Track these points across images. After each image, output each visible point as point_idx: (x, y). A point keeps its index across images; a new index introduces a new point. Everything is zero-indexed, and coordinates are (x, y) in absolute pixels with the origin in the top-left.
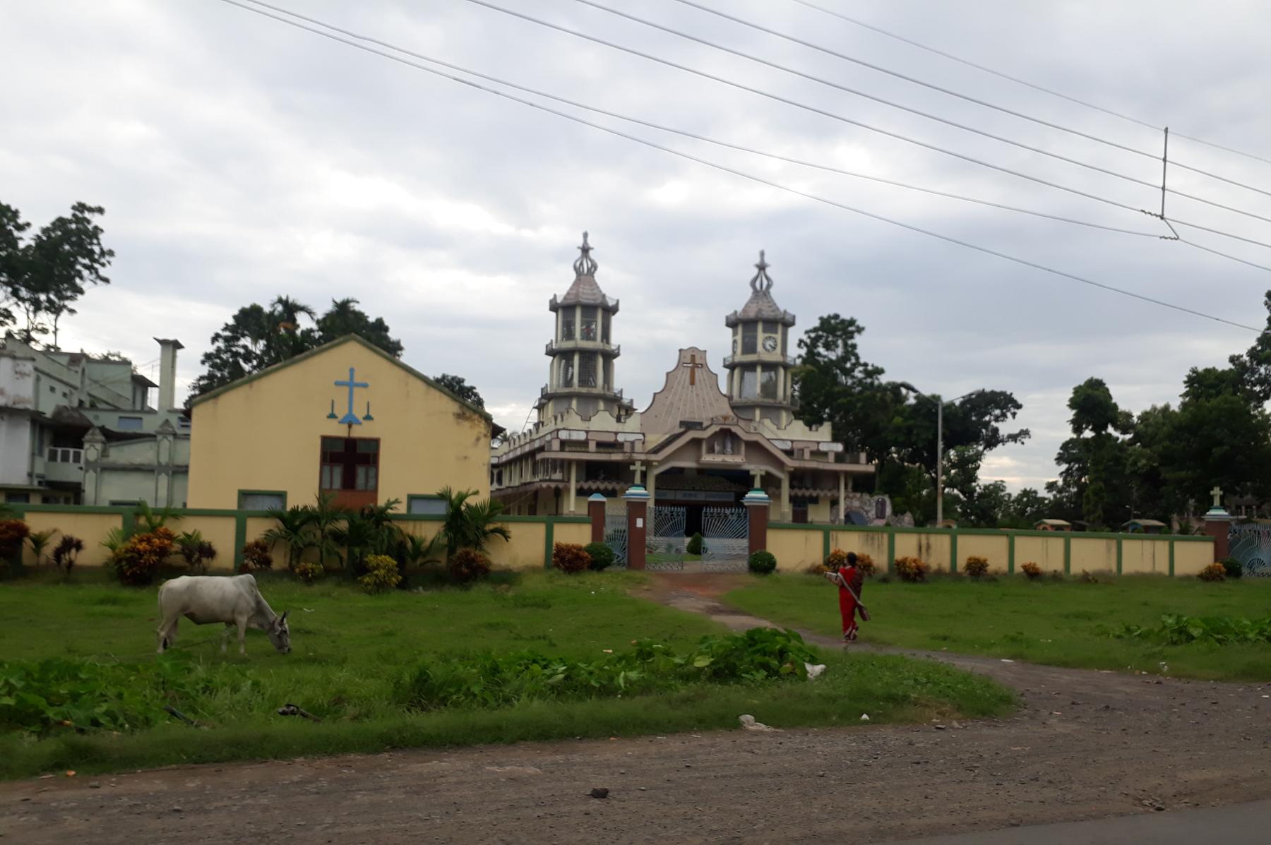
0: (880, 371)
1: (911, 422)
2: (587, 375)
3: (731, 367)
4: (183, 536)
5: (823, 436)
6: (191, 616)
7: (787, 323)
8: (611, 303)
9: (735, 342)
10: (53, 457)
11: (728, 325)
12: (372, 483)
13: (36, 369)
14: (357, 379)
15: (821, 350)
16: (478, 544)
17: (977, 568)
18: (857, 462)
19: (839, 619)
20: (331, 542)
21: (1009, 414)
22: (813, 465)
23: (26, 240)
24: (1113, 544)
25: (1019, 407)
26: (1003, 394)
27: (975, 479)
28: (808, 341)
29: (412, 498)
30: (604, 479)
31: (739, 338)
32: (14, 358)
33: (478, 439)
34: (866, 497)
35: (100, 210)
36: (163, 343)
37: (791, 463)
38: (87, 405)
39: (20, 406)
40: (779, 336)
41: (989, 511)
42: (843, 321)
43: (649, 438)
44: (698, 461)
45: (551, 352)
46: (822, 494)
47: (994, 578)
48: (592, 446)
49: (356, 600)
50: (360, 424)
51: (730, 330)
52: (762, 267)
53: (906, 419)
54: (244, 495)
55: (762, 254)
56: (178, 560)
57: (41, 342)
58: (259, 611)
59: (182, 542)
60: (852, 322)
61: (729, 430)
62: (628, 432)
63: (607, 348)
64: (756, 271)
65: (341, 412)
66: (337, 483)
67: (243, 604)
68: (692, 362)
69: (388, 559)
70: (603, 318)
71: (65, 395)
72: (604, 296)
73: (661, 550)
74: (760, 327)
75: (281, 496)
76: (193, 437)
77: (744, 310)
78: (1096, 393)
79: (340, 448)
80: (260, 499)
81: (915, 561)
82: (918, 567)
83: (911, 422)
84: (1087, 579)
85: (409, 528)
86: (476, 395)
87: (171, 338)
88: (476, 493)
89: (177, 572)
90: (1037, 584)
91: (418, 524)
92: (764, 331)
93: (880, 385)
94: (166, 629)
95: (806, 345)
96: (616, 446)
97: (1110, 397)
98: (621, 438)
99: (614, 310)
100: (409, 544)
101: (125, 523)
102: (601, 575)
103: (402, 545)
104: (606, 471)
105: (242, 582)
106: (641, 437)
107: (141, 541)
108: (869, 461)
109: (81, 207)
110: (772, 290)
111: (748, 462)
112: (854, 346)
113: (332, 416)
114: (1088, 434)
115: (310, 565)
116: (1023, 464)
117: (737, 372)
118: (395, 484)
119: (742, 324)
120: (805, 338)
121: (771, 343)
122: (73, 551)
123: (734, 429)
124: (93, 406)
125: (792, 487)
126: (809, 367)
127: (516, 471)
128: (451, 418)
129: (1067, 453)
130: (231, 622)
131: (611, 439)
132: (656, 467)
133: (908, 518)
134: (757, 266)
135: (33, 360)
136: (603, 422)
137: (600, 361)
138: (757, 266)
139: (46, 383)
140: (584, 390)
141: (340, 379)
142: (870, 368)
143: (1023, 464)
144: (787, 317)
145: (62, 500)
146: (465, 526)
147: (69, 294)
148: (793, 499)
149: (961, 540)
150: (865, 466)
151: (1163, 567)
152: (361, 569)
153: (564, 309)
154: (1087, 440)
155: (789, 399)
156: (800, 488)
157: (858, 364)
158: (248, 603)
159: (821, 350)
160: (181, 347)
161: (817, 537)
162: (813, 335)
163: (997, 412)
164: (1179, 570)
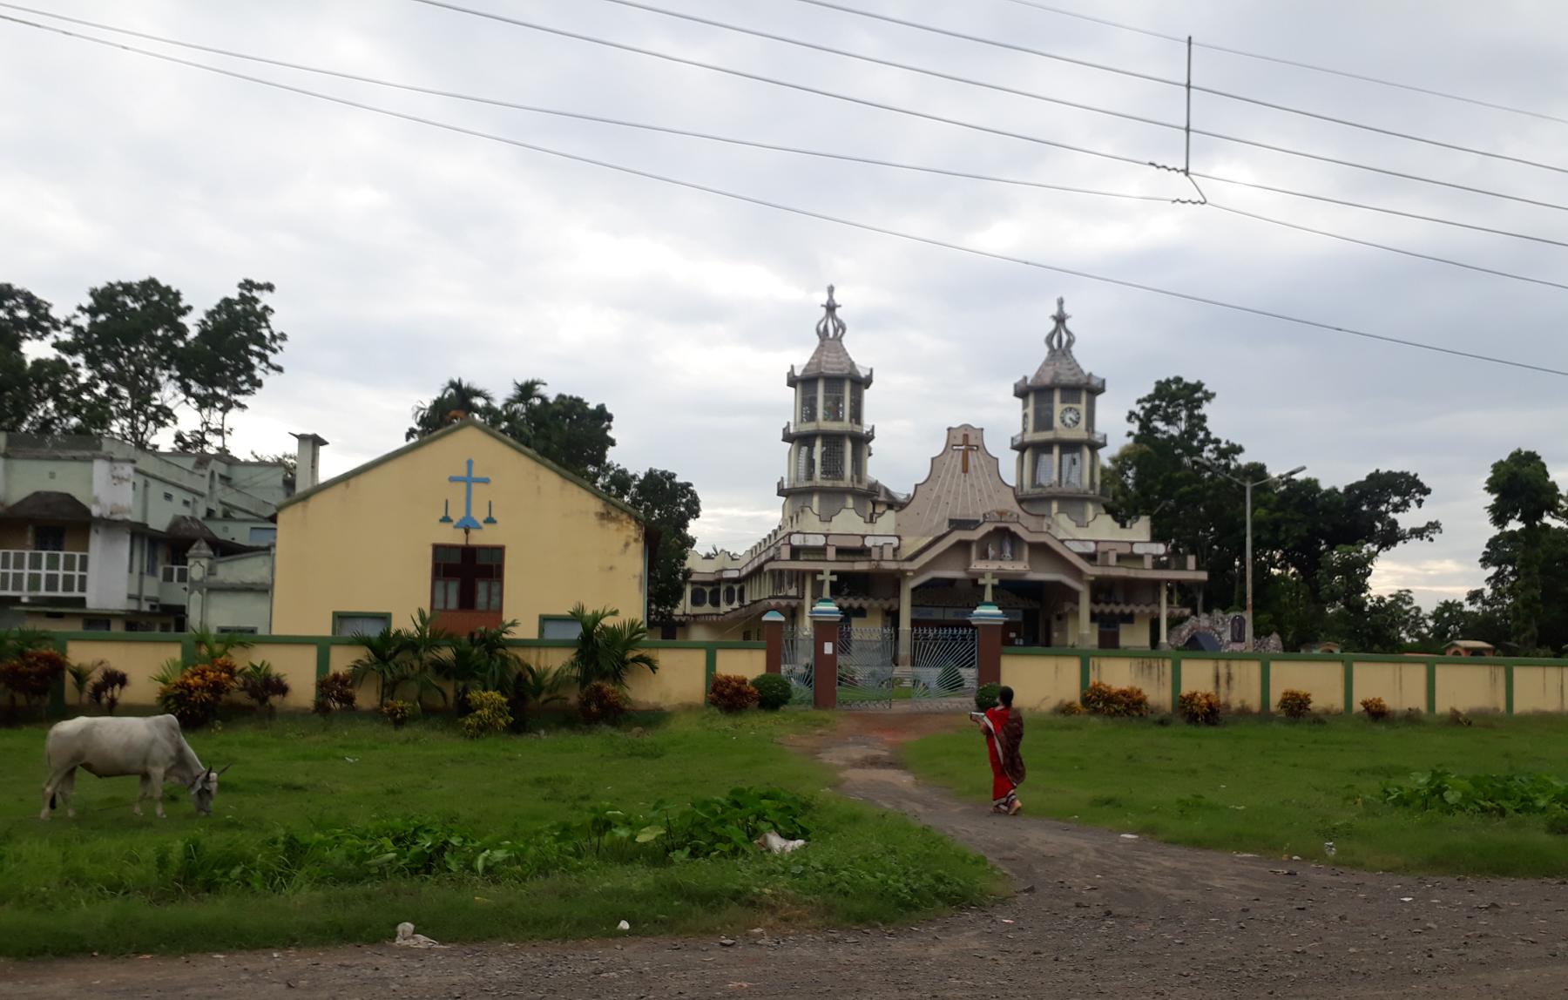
0: (1240, 450)
1: (1278, 515)
2: (832, 466)
3: (1021, 448)
4: (249, 669)
5: (1139, 532)
6: (88, 767)
7: (1093, 389)
8: (863, 374)
9: (1025, 416)
10: (168, 577)
11: (1016, 395)
12: (495, 600)
13: (137, 471)
14: (475, 474)
15: (1160, 425)
16: (617, 677)
17: (1296, 706)
18: (1183, 567)
19: (987, 776)
20: (429, 675)
21: (1412, 503)
22: (1122, 572)
23: (192, 324)
24: (1500, 672)
25: (1427, 492)
26: (1404, 475)
27: (1365, 588)
28: (1141, 413)
29: (545, 619)
30: (849, 595)
31: (1030, 411)
32: (111, 460)
33: (627, 545)
34: (1218, 613)
35: (270, 287)
36: (302, 438)
37: (1091, 571)
38: (219, 514)
39: (118, 517)
40: (1082, 407)
41: (1379, 631)
42: (1187, 385)
43: (906, 541)
44: (966, 570)
45: (788, 437)
46: (1137, 610)
47: (1321, 720)
48: (831, 553)
49: (443, 745)
50: (480, 528)
51: (1020, 401)
52: (1060, 319)
53: (1272, 511)
54: (340, 618)
55: (1061, 302)
56: (242, 698)
57: (214, 443)
58: (181, 761)
59: (248, 675)
60: (1198, 387)
61: (1006, 530)
62: (882, 532)
63: (857, 429)
64: (824, 310)
65: (457, 514)
66: (453, 603)
67: (157, 753)
68: (965, 444)
69: (496, 695)
70: (853, 391)
71: (186, 503)
72: (852, 364)
73: (908, 684)
74: (1057, 396)
75: (385, 618)
76: (279, 550)
77: (1038, 375)
78: (1526, 470)
79: (456, 559)
80: (359, 622)
81: (1207, 696)
82: (1210, 705)
83: (1278, 515)
84: (1456, 720)
85: (532, 658)
86: (693, 493)
87: (310, 432)
88: (615, 613)
89: (70, 713)
90: (1381, 727)
91: (543, 651)
92: (1063, 401)
93: (1239, 467)
94: (55, 780)
95: (1138, 417)
96: (863, 552)
97: (1547, 475)
98: (869, 542)
99: (867, 382)
100: (530, 678)
101: (184, 653)
102: (776, 715)
103: (520, 678)
104: (863, 585)
105: (158, 724)
106: (895, 541)
107: (194, 674)
108: (1198, 568)
109: (248, 285)
110: (1074, 349)
111: (1033, 570)
112: (1203, 418)
113: (446, 519)
114: (1515, 525)
115: (400, 703)
116: (1434, 566)
117: (1027, 455)
118: (525, 604)
119: (1034, 393)
120: (1137, 409)
121: (1070, 416)
122: (117, 687)
123: (1014, 528)
124: (227, 516)
125: (1094, 600)
126: (1145, 447)
127: (755, 584)
128: (593, 520)
129: (1494, 554)
130: (146, 777)
131: (857, 543)
132: (912, 578)
133: (1274, 640)
134: (1054, 318)
135: (133, 461)
136: (849, 523)
137: (848, 446)
138: (1054, 318)
139: (156, 489)
140: (828, 484)
141: (454, 474)
142: (1223, 445)
143: (1434, 566)
144: (1094, 382)
145: (158, 627)
146: (602, 650)
147: (246, 387)
148: (1094, 617)
149: (1275, 668)
150: (1192, 572)
151: (1417, 701)
152: (465, 707)
153: (803, 383)
154: (1512, 532)
155: (1098, 489)
156: (1107, 603)
157: (1207, 439)
158: (164, 750)
159: (1160, 425)
160: (324, 443)
161: (1072, 667)
162: (1148, 405)
163: (1396, 499)
164: (1518, 707)
